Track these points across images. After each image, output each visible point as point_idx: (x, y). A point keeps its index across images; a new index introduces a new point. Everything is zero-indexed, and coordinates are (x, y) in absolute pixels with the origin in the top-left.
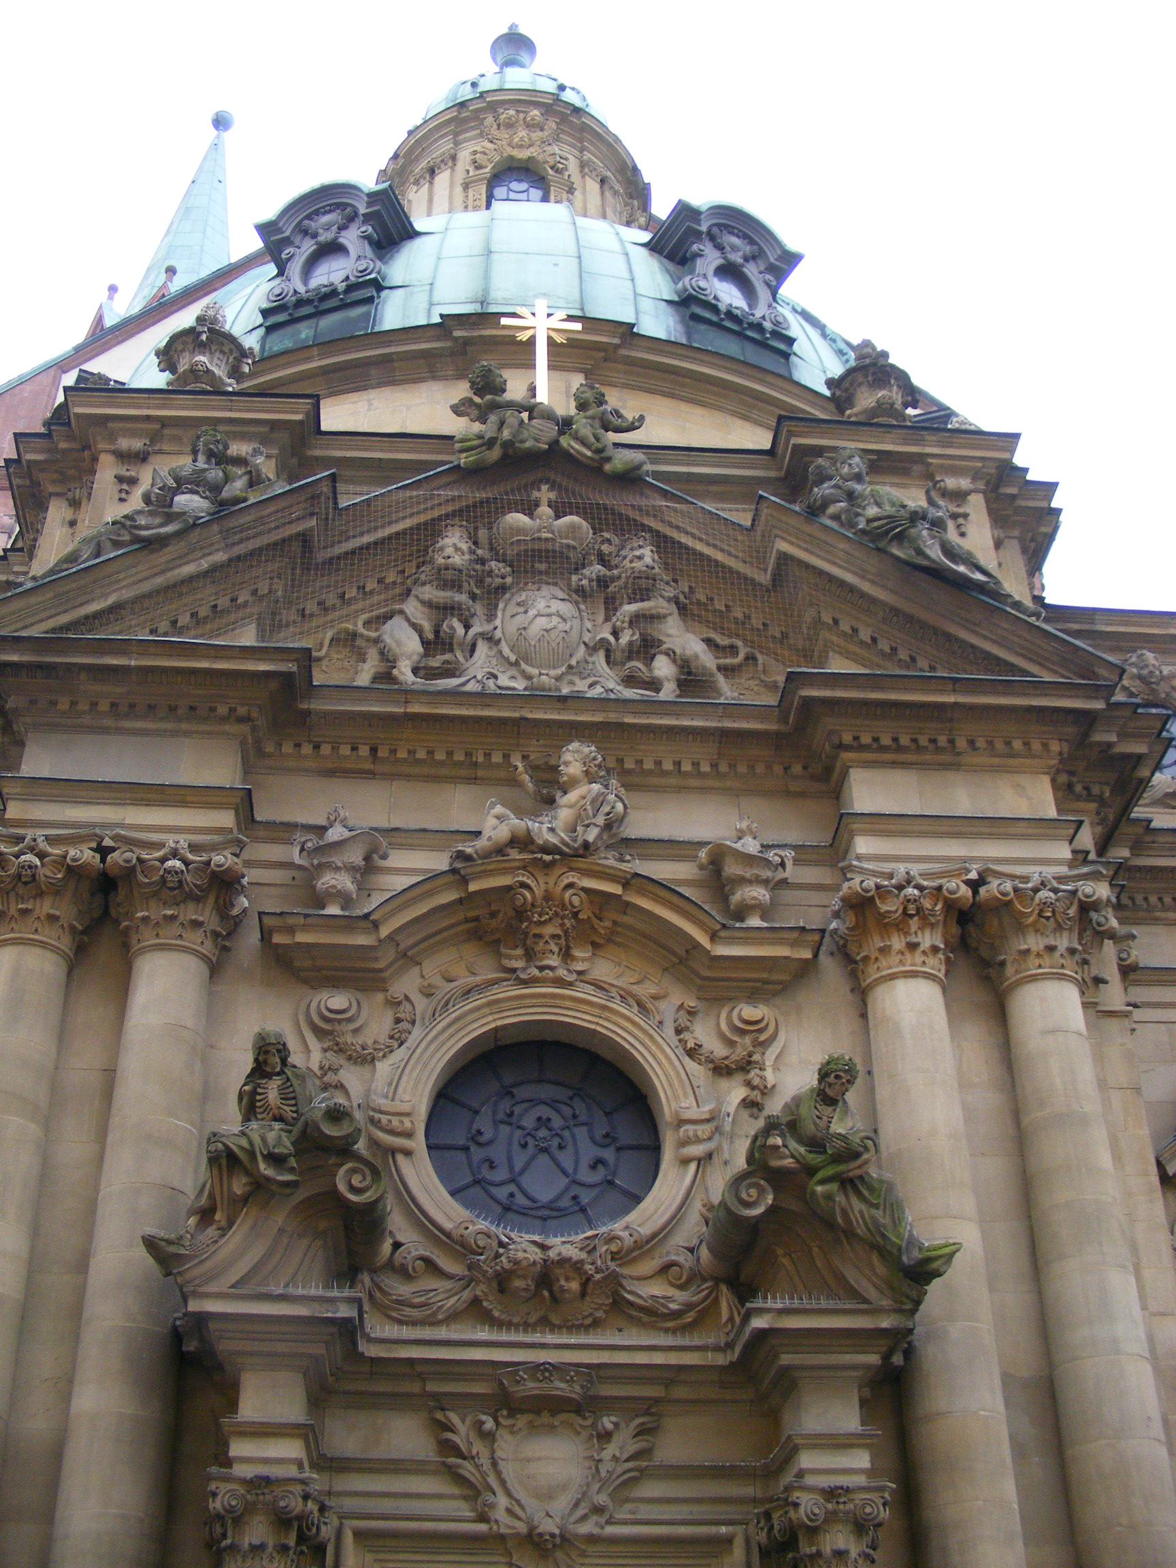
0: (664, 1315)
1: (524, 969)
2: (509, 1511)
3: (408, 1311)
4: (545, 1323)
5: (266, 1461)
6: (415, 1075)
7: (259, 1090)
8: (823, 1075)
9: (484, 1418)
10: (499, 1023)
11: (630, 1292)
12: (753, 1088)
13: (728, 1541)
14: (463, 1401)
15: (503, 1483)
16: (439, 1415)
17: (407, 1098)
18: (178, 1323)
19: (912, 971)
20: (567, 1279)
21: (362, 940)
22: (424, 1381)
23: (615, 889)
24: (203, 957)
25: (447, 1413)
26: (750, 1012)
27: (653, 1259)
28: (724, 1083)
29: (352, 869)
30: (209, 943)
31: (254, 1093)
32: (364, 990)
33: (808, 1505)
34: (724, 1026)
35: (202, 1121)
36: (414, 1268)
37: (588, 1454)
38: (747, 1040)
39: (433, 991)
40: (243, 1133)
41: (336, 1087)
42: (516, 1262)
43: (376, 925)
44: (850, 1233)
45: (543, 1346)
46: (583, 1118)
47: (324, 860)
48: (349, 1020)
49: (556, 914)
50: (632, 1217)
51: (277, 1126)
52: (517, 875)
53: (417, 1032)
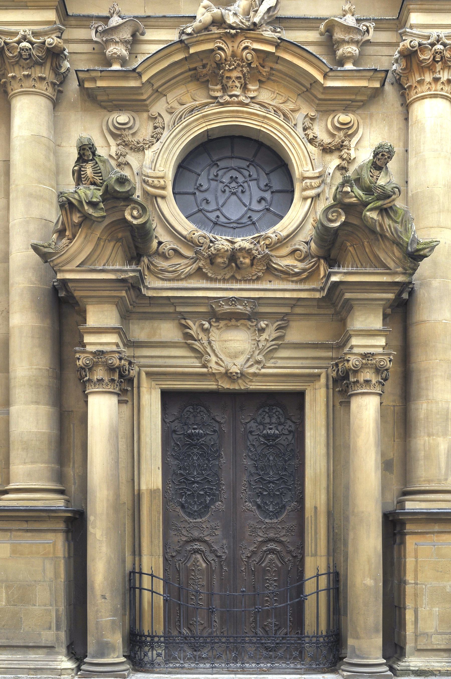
0: (293, 274)
1: (222, 97)
2: (217, 363)
3: (167, 274)
4: (233, 278)
5: (101, 344)
6: (165, 156)
7: (82, 169)
8: (376, 154)
9: (204, 322)
10: (209, 127)
11: (275, 264)
12: (344, 160)
13: (319, 375)
14: (195, 315)
15: (214, 351)
16: (183, 322)
17: (162, 169)
18: (55, 284)
19: (435, 94)
20: (244, 258)
21: (133, 84)
22: (175, 306)
23: (271, 49)
24: (48, 97)
25: (187, 321)
26: (343, 118)
27: (287, 247)
28: (328, 158)
29: (125, 42)
30: (50, 89)
31: (80, 170)
32: (136, 111)
33: (353, 361)
34: (330, 126)
35: (57, 185)
36: (169, 254)
37: (253, 338)
38: (342, 134)
39: (173, 110)
40: (76, 192)
41: (125, 164)
42: (219, 250)
43: (140, 75)
44: (383, 236)
45: (231, 289)
46: (255, 176)
47: (109, 38)
48: (130, 128)
49: (238, 65)
50: (278, 227)
51: (92, 187)
52: (217, 43)
53: (166, 133)
